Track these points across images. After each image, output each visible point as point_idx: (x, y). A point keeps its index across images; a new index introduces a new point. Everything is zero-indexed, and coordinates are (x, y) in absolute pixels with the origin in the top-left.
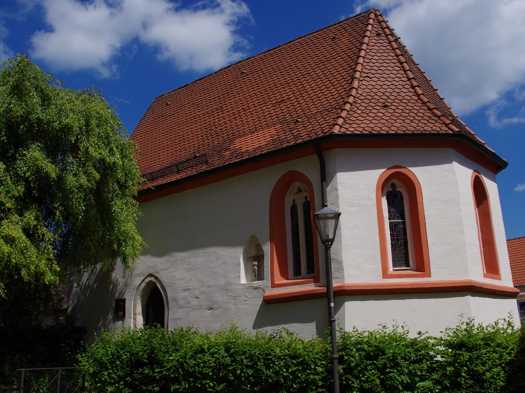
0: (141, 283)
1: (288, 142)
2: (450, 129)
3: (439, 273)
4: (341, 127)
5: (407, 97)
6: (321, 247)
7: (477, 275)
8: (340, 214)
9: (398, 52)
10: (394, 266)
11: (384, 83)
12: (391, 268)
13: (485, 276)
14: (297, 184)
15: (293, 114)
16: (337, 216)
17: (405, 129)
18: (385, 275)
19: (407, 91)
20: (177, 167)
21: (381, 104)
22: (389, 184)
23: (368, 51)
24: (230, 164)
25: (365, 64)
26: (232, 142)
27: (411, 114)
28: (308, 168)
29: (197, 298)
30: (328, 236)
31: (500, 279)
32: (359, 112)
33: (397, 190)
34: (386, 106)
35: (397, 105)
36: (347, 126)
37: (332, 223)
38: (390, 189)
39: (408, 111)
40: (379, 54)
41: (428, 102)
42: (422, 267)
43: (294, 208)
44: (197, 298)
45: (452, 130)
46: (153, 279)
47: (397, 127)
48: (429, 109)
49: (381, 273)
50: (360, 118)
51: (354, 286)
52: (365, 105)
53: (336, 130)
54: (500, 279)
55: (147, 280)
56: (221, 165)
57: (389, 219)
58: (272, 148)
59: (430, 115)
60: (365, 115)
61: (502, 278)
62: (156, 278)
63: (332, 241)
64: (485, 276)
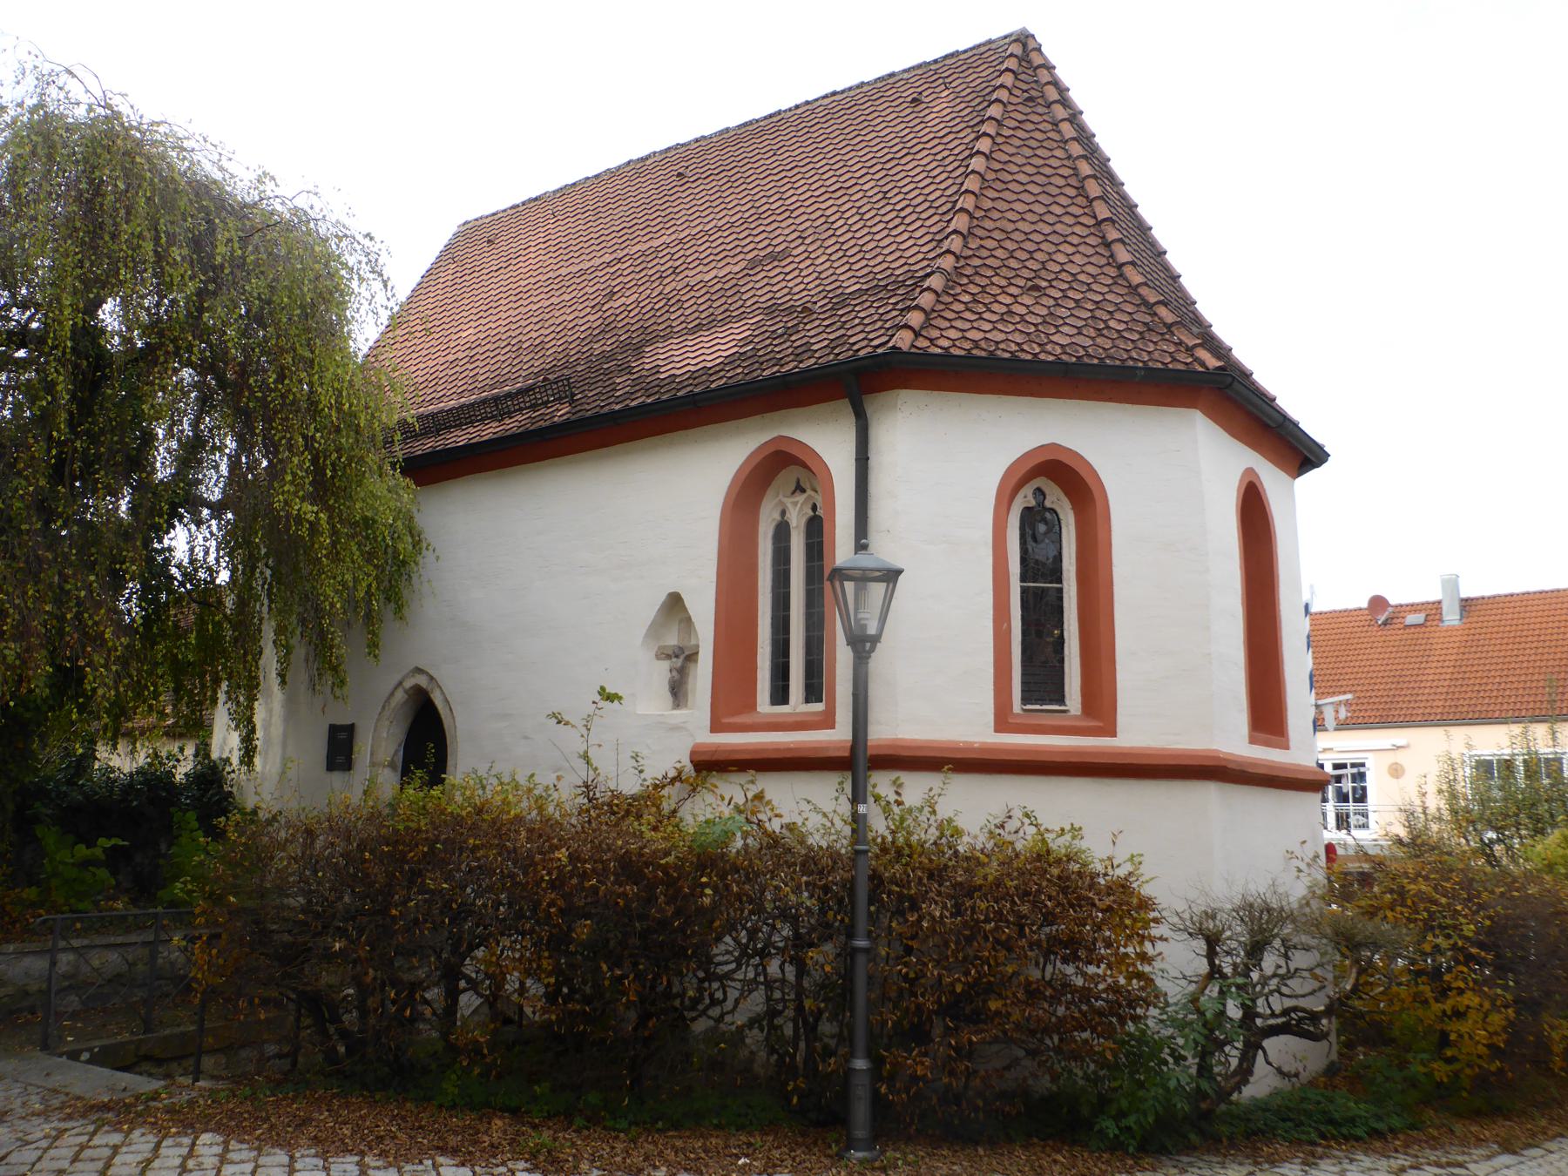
0: (396, 688)
1: (779, 362)
2: (1197, 360)
3: (1137, 730)
4: (917, 334)
5: (1090, 269)
6: (843, 657)
7: (1231, 737)
8: (899, 572)
9: (1076, 150)
10: (1025, 700)
11: (1033, 227)
12: (1017, 707)
13: (1253, 741)
14: (788, 476)
15: (796, 290)
16: (891, 576)
17: (1082, 352)
18: (1003, 721)
19: (1091, 251)
20: (497, 406)
21: (1021, 283)
22: (1028, 490)
23: (999, 140)
24: (628, 409)
25: (990, 176)
26: (638, 350)
27: (1004, 283)
28: (828, 441)
29: (526, 738)
30: (864, 627)
31: (1287, 748)
32: (966, 298)
33: (1048, 504)
34: (1036, 288)
35: (1066, 286)
36: (935, 333)
37: (877, 590)
38: (1033, 503)
39: (1090, 306)
40: (1028, 152)
41: (1145, 284)
42: (1100, 707)
43: (782, 533)
44: (526, 738)
45: (1203, 364)
46: (422, 681)
47: (1064, 342)
48: (1145, 303)
49: (992, 717)
50: (968, 315)
51: (919, 748)
52: (984, 282)
53: (903, 340)
54: (1287, 748)
55: (408, 684)
56: (606, 410)
57: (1023, 580)
58: (738, 374)
59: (1148, 319)
60: (981, 308)
61: (1292, 744)
62: (432, 678)
63: (875, 640)
64: (1253, 741)
